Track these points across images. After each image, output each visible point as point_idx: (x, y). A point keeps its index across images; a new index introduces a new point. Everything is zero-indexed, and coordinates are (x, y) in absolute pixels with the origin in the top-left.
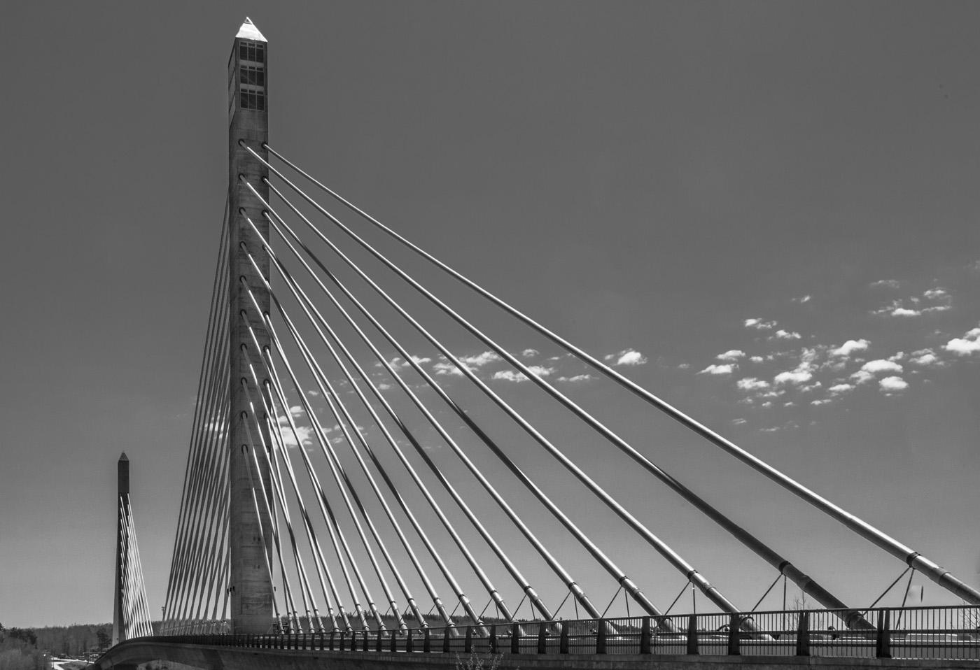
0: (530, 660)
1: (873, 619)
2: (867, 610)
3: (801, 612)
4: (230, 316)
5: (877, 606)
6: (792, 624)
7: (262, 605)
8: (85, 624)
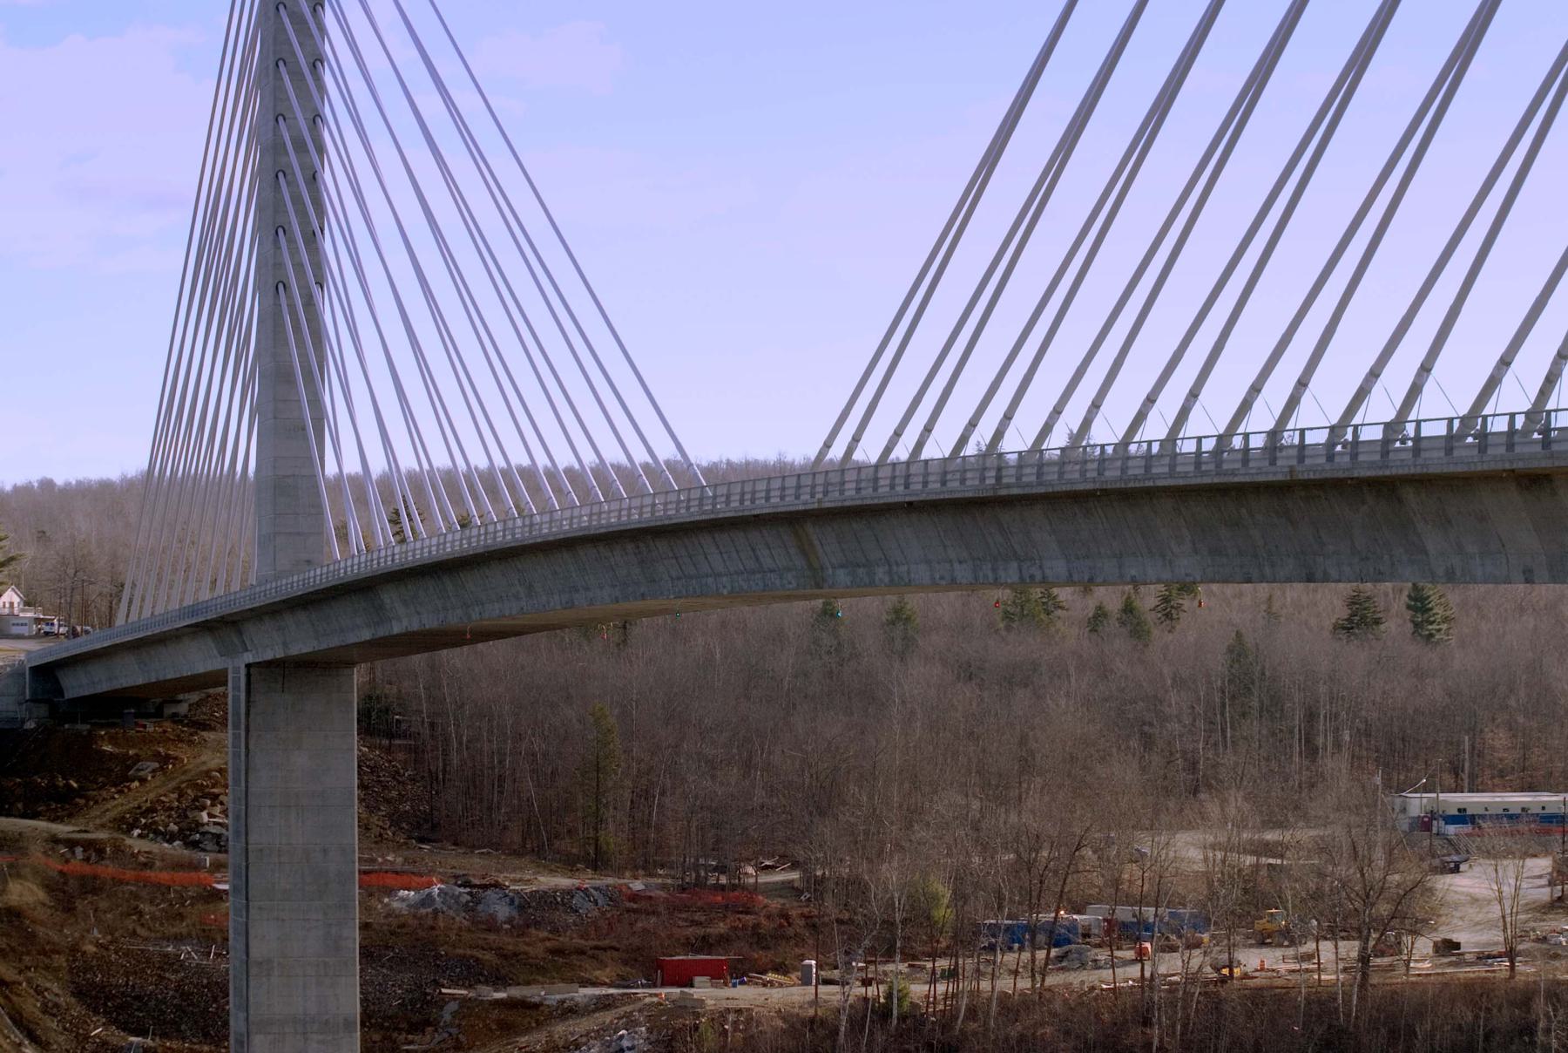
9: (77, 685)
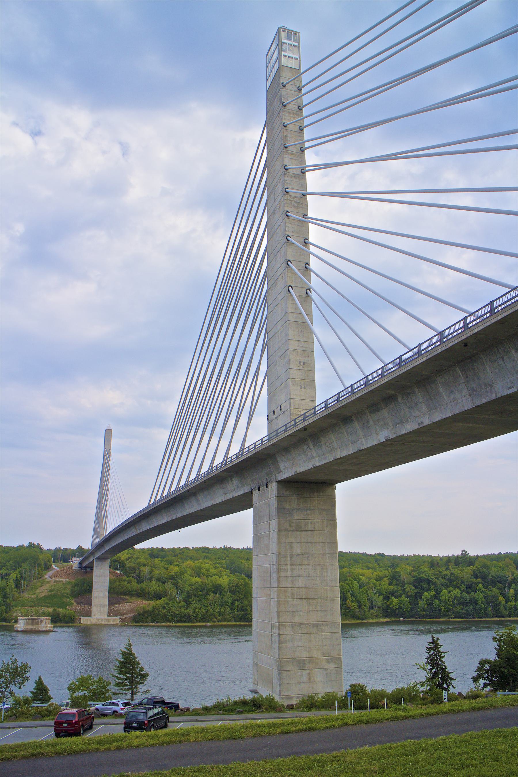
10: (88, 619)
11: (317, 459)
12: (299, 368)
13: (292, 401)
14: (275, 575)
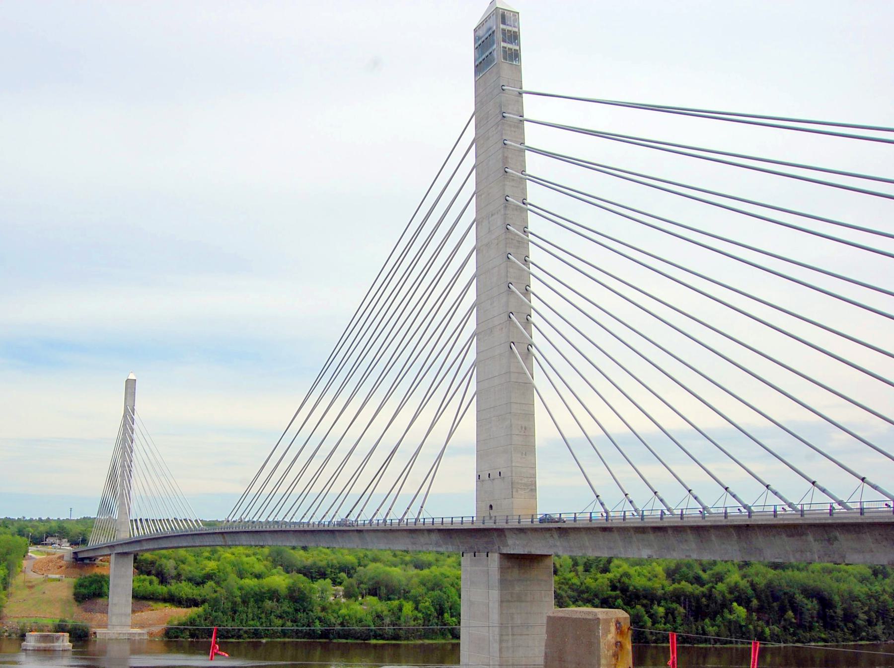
0: (802, 551)
1: (799, 507)
2: (797, 505)
3: (830, 503)
4: (521, 325)
5: (800, 503)
6: (363, 522)
7: (528, 490)
8: (215, 519)
9: (81, 556)
10: (106, 633)
11: (560, 548)
12: (520, 434)
13: (514, 468)
14: (496, 646)
